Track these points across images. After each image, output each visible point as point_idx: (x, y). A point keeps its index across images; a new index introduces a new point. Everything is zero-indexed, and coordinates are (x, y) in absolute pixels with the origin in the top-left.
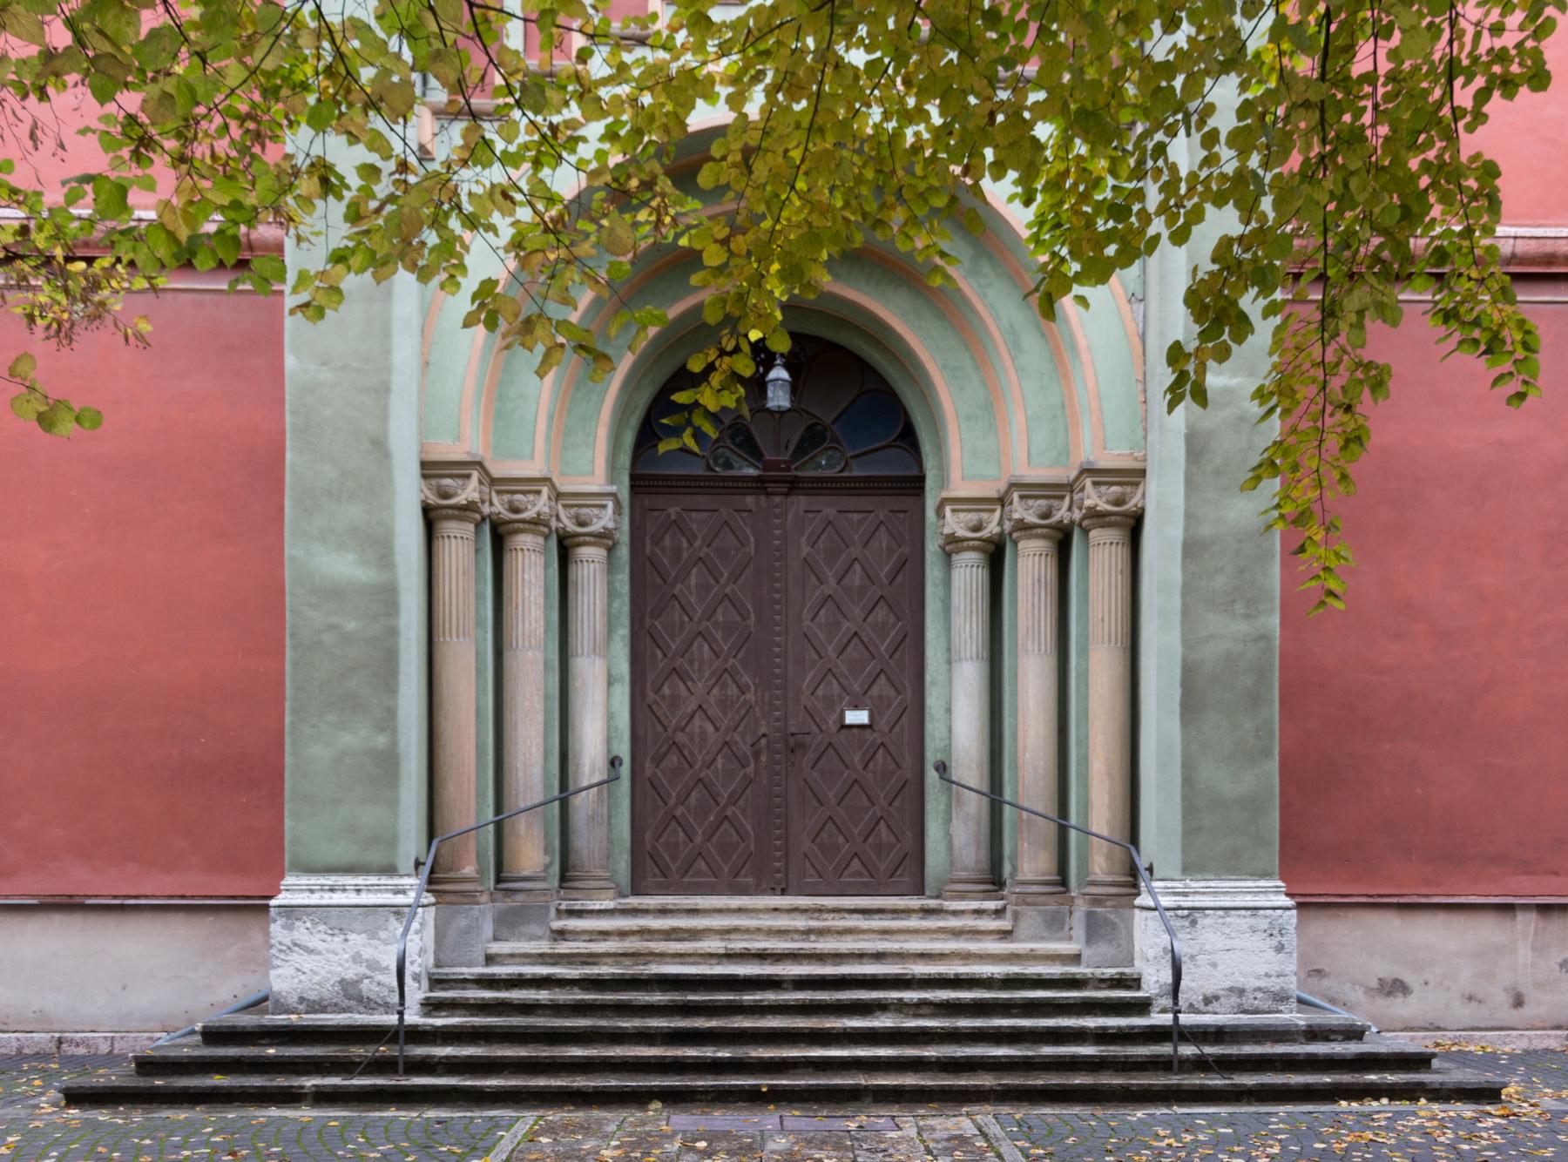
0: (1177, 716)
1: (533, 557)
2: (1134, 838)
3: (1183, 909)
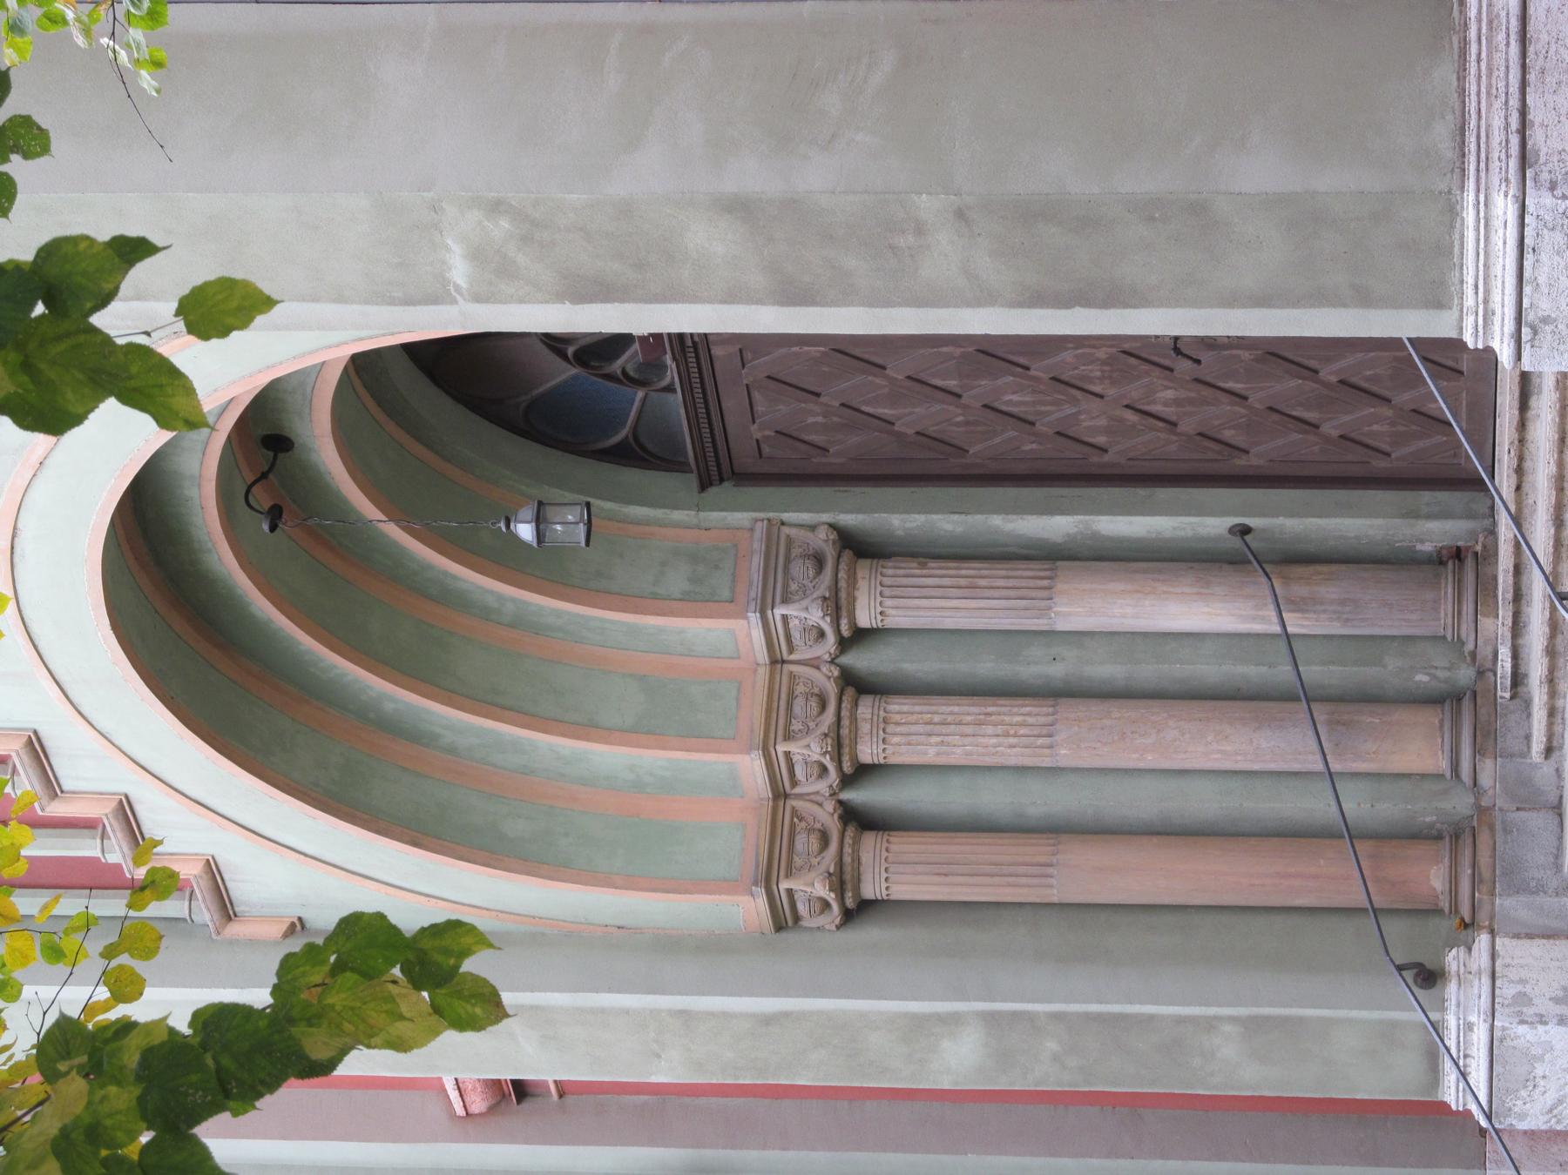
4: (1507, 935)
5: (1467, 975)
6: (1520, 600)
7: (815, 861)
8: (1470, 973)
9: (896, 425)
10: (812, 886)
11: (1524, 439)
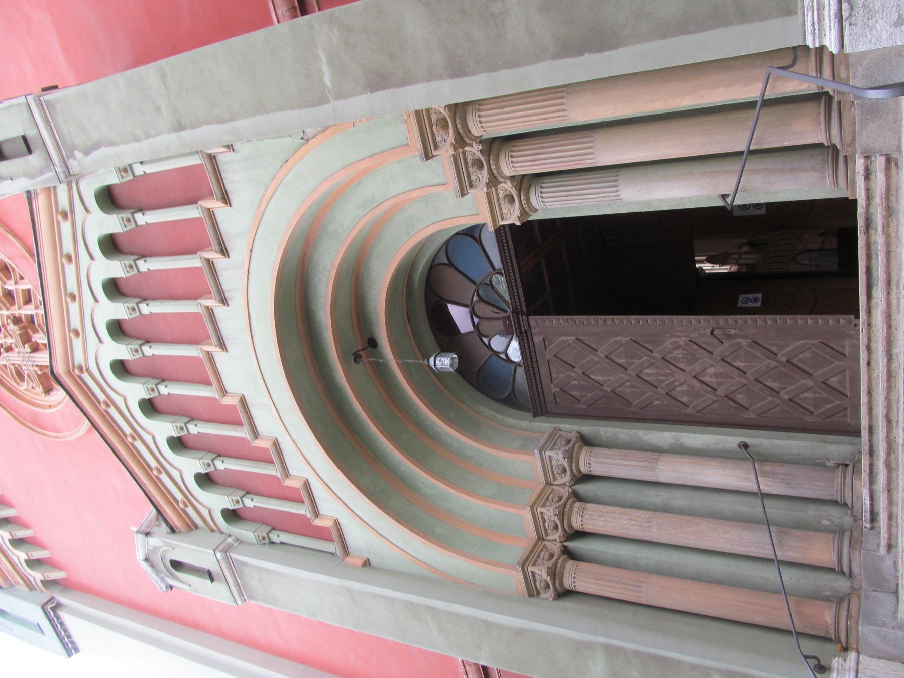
0: (612, 52)
1: (587, 517)
2: (748, 106)
3: (840, 9)
4: (866, 654)
5: (842, 671)
6: (873, 455)
7: (545, 563)
8: (845, 670)
9: (604, 386)
10: (542, 572)
11: (870, 323)
